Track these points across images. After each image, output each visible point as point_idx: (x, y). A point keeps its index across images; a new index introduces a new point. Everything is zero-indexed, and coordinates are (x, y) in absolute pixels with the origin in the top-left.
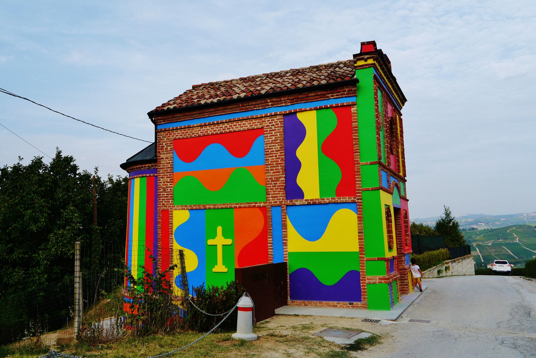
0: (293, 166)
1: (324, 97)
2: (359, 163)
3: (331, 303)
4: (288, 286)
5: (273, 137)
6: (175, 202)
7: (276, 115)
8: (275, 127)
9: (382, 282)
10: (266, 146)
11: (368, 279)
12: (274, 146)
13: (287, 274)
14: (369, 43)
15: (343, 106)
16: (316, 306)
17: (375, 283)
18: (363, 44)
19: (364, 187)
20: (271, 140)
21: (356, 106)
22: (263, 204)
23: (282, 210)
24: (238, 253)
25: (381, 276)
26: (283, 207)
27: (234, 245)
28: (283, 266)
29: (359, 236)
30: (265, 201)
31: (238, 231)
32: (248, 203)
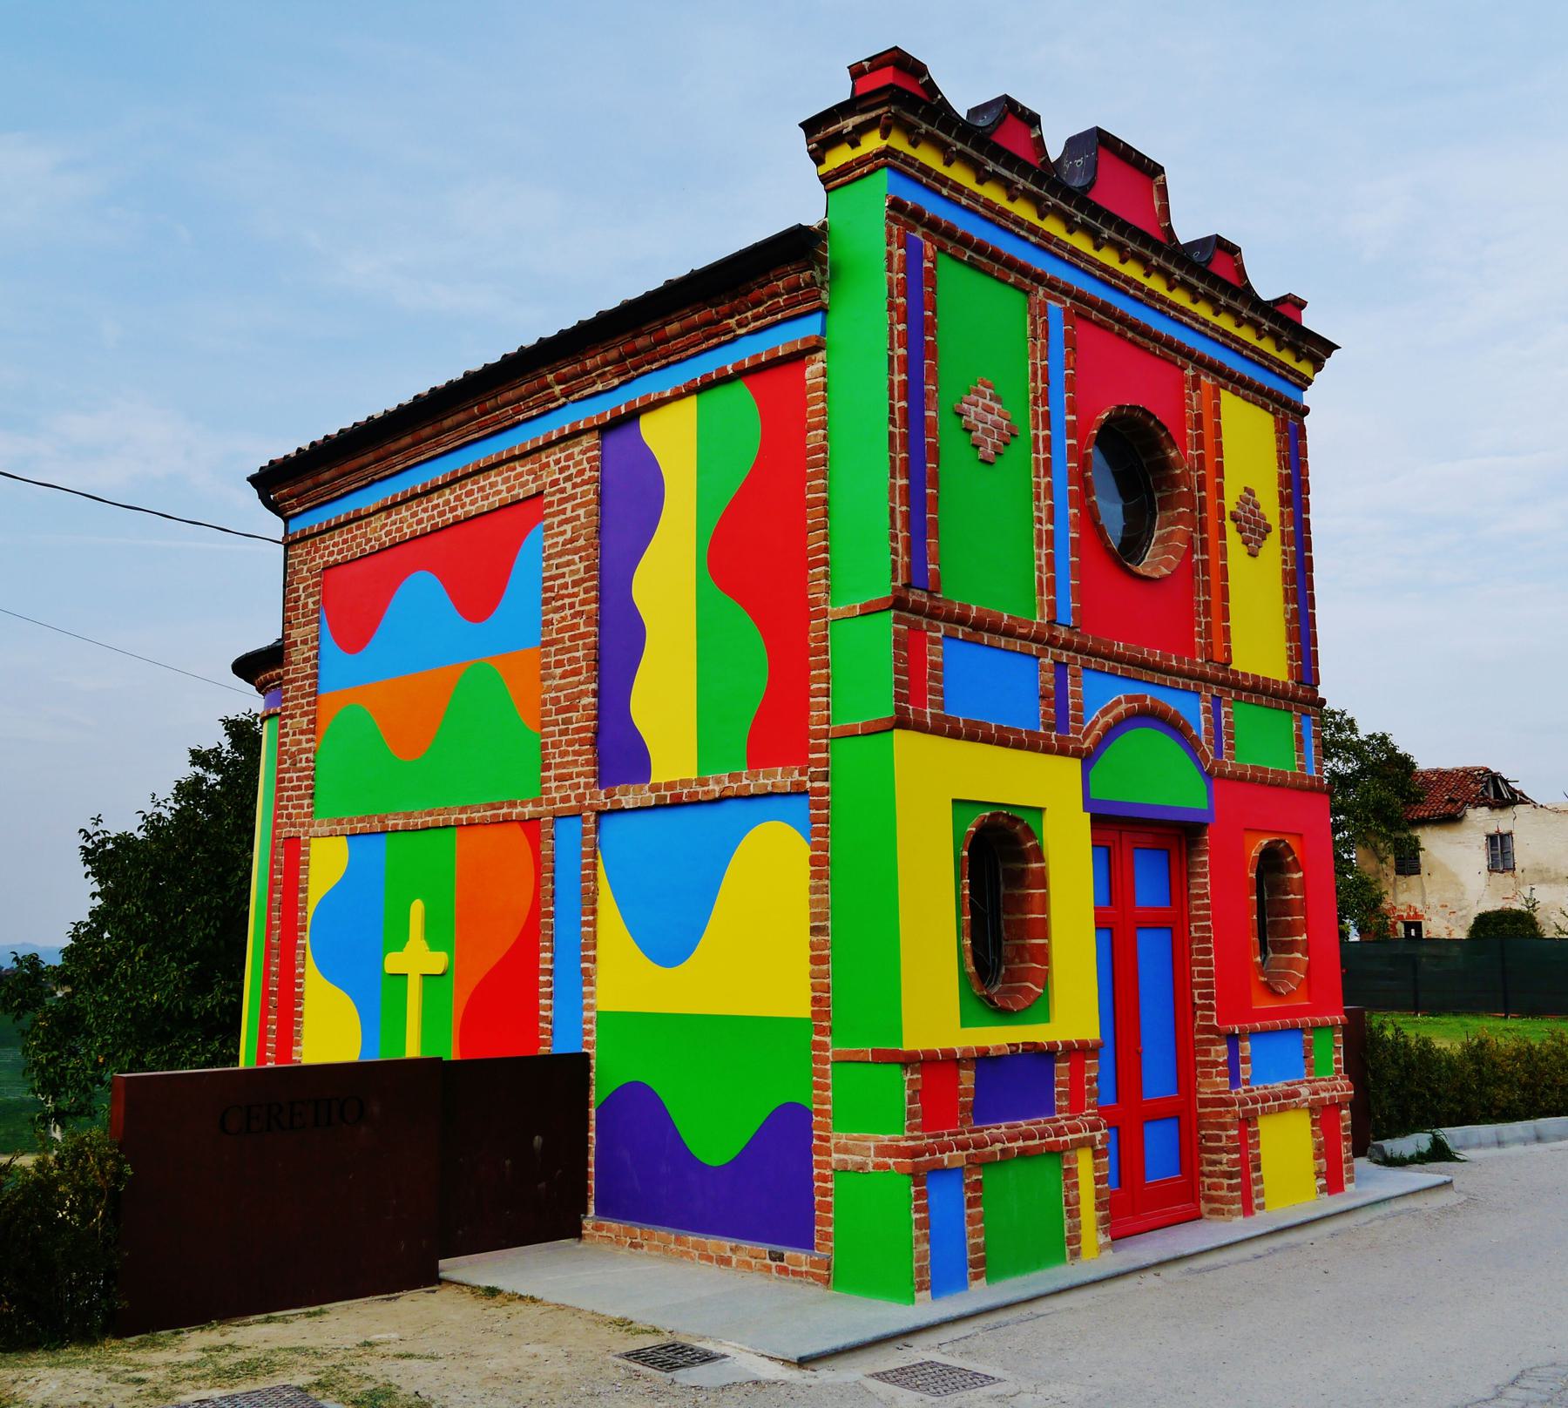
0: (618, 642)
1: (715, 335)
2: (824, 613)
3: (714, 1243)
4: (592, 1158)
5: (568, 527)
6: (319, 807)
7: (576, 434)
8: (575, 486)
9: (887, 1167)
10: (549, 568)
11: (838, 1150)
12: (568, 564)
13: (587, 1104)
14: (878, 61)
15: (776, 363)
16: (960, 899)
17: (861, 1167)
18: (857, 72)
20: (561, 539)
21: (820, 356)
22: (530, 808)
23: (585, 832)
24: (465, 998)
25: (885, 1139)
26: (586, 820)
27: (451, 976)
28: (578, 1064)
29: (813, 946)
30: (537, 795)
31: (463, 923)
32: (492, 806)
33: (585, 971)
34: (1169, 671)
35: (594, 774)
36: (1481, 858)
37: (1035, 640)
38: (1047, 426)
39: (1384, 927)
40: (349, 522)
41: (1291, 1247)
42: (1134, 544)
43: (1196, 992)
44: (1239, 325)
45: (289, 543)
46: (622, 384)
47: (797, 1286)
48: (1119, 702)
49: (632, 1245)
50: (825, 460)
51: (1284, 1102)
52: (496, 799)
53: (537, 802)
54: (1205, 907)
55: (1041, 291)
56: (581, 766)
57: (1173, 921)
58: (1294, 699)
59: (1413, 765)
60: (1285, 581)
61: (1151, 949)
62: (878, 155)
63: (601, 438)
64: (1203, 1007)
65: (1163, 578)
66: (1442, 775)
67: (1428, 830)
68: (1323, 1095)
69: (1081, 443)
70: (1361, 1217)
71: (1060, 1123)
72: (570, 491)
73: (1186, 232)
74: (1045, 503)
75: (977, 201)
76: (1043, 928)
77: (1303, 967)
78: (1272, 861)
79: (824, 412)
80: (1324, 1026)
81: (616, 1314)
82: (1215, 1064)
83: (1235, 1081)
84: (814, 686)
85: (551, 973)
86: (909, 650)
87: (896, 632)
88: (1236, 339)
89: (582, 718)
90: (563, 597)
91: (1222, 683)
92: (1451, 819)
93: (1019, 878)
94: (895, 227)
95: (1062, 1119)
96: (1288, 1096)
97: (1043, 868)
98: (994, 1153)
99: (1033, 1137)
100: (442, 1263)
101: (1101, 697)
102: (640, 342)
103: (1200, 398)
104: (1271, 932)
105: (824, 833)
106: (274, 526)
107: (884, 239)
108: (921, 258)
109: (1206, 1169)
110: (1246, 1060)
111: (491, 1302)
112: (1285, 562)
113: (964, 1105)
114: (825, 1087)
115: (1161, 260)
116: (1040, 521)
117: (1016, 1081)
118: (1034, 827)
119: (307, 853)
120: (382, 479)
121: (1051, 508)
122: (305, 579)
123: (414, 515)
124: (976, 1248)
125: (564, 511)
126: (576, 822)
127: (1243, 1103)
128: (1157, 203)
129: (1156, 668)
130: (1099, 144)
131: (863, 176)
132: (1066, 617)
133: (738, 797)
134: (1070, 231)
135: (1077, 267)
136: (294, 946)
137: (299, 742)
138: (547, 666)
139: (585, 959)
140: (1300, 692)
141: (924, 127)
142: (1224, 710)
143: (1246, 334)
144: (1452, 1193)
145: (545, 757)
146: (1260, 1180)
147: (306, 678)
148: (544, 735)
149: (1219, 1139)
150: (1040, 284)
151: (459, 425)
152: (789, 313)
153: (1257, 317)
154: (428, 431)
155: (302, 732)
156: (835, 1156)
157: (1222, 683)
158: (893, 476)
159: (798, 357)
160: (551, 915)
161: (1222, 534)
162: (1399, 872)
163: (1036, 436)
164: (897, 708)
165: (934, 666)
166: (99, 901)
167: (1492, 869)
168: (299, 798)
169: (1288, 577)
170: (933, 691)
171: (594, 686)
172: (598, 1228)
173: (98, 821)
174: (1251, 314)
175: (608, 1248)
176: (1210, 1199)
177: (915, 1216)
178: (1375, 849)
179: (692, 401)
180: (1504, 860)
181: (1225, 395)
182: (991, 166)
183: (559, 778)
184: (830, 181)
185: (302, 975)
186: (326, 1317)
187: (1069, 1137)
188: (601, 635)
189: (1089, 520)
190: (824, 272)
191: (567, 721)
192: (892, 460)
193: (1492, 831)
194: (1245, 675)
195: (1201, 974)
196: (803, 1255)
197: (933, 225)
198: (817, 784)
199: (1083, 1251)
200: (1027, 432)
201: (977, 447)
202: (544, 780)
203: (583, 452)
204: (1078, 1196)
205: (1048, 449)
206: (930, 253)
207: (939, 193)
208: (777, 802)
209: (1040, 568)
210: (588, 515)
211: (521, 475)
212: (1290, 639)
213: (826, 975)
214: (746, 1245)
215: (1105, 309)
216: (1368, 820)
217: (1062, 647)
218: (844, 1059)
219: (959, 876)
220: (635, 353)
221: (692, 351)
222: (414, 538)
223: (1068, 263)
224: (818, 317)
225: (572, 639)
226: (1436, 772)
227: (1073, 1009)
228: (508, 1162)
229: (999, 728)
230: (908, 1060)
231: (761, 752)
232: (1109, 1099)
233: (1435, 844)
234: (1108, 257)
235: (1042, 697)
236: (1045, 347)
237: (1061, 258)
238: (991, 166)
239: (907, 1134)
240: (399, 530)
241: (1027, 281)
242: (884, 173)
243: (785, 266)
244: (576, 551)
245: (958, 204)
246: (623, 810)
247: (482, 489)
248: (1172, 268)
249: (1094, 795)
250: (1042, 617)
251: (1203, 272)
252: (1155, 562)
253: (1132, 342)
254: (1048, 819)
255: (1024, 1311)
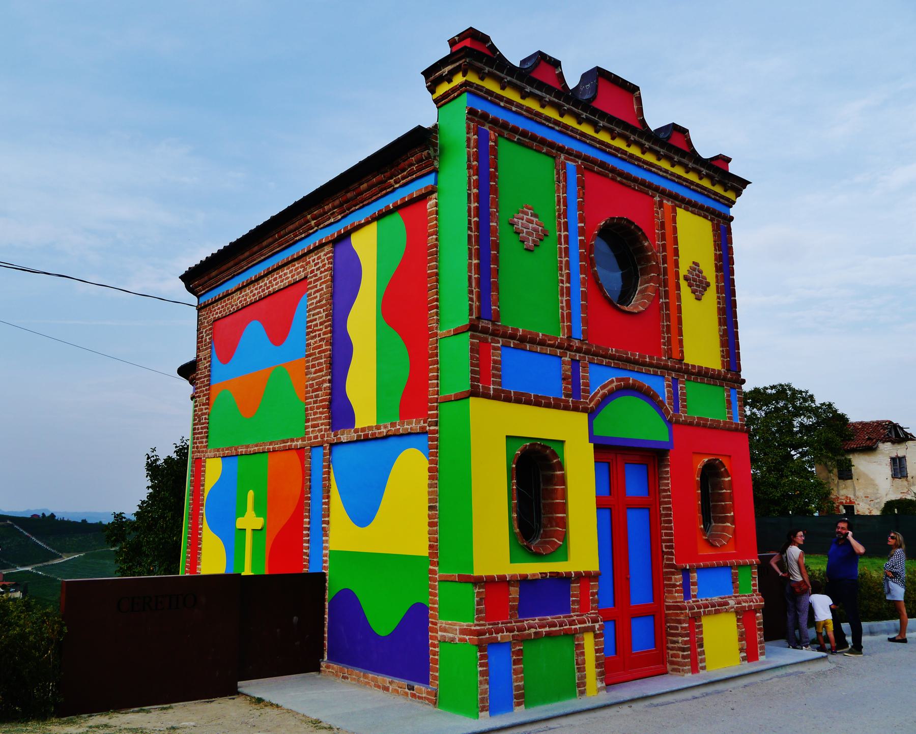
1: (385, 189)
2: (436, 335)
4: (326, 629)
5: (318, 294)
7: (321, 246)
8: (321, 273)
9: (465, 640)
13: (324, 600)
14: (463, 36)
16: (510, 491)
17: (452, 640)
18: (452, 43)
19: (444, 393)
20: (315, 301)
21: (434, 196)
23: (325, 455)
25: (464, 624)
26: (325, 448)
27: (265, 529)
28: (320, 579)
29: (430, 517)
31: (270, 505)
32: (284, 441)
33: (324, 529)
34: (644, 364)
35: (329, 424)
36: (887, 471)
37: (559, 347)
38: (566, 229)
39: (832, 508)
40: (224, 297)
41: (718, 692)
42: (626, 295)
43: (664, 545)
44: (687, 172)
45: (200, 309)
46: (343, 218)
47: (420, 705)
48: (612, 382)
49: (344, 677)
50: (437, 252)
51: (719, 609)
52: (285, 438)
53: (303, 439)
54: (669, 496)
55: (562, 157)
56: (322, 419)
57: (650, 505)
58: (725, 379)
59: (847, 420)
60: (719, 314)
61: (636, 521)
62: (462, 85)
63: (334, 247)
64: (668, 553)
65: (640, 313)
66: (864, 425)
67: (856, 455)
68: (744, 604)
69: (587, 239)
70: (765, 676)
71: (574, 618)
72: (319, 276)
73: (654, 123)
74: (565, 272)
75: (522, 109)
76: (564, 508)
77: (731, 531)
78: (711, 472)
79: (436, 226)
80: (745, 565)
81: (314, 717)
82: (674, 586)
83: (687, 596)
84: (431, 374)
85: (308, 529)
86: (479, 354)
87: (472, 344)
88: (686, 180)
89: (323, 395)
90: (315, 331)
91: (679, 370)
92: (869, 449)
93: (550, 480)
94: (472, 124)
95: (574, 616)
96: (720, 605)
97: (563, 474)
98: (530, 635)
99: (555, 626)
100: (240, 683)
101: (600, 379)
102: (349, 195)
103: (663, 212)
104: (710, 509)
105: (435, 454)
106: (194, 300)
107: (465, 130)
108: (488, 140)
109: (671, 645)
110: (694, 584)
111: (256, 707)
112: (719, 303)
113: (513, 607)
114: (435, 595)
115: (636, 138)
116: (562, 282)
117: (547, 594)
118: (557, 451)
119: (204, 466)
120: (238, 274)
121: (568, 275)
122: (206, 327)
123: (252, 292)
124: (518, 688)
125: (316, 286)
126: (320, 449)
127: (691, 608)
128: (635, 107)
129: (636, 362)
130: (598, 76)
131: (455, 98)
132: (578, 333)
133: (394, 435)
134: (580, 123)
135: (585, 143)
136: (198, 514)
137: (202, 410)
138: (308, 368)
139: (324, 522)
140: (730, 373)
141: (487, 69)
142: (680, 386)
143: (692, 177)
144: (827, 663)
145: (307, 415)
146: (703, 653)
147: (205, 377)
148: (307, 404)
149: (677, 628)
150: (544, 145)
151: (270, 244)
152: (419, 174)
153: (698, 167)
154: (256, 248)
155: (204, 405)
156: (440, 633)
157: (679, 370)
158: (470, 258)
159: (423, 197)
160: (309, 498)
161: (678, 287)
162: (840, 478)
163: (560, 235)
164: (472, 386)
165: (495, 362)
166: (151, 490)
167: (894, 476)
168: (202, 438)
169: (721, 311)
170: (494, 376)
171: (329, 377)
172: (328, 667)
173: (154, 450)
174: (695, 166)
175: (332, 678)
176: (672, 663)
177: (479, 669)
178: (826, 464)
179: (374, 226)
180: (901, 471)
181: (680, 211)
182: (528, 89)
183: (314, 426)
184: (440, 102)
185: (201, 529)
186: (170, 711)
187: (578, 626)
188: (333, 350)
189: (594, 281)
190: (435, 151)
191: (317, 396)
192: (470, 250)
193: (894, 455)
194: (693, 366)
195: (666, 534)
196: (423, 688)
197: (495, 122)
198: (432, 428)
199: (587, 691)
200: (554, 233)
201: (523, 242)
202: (307, 427)
203: (325, 255)
204: (584, 660)
205: (567, 242)
206: (493, 137)
207: (499, 105)
208: (413, 438)
209: (562, 308)
210: (327, 287)
211: (297, 268)
212: (722, 345)
213: (436, 532)
214: (396, 680)
215: (602, 165)
216: (821, 450)
217: (575, 351)
218: (445, 580)
219: (510, 478)
220: (346, 201)
221: (375, 198)
222: (252, 304)
223: (580, 140)
224: (433, 176)
225: (319, 353)
226: (861, 423)
227: (583, 551)
228: (278, 630)
229: (536, 396)
230: (477, 581)
231: (406, 412)
232: (608, 603)
233: (861, 463)
234: (604, 137)
235: (564, 379)
236: (565, 187)
237: (575, 138)
238: (528, 89)
239: (476, 622)
240: (245, 300)
241: (554, 151)
242: (465, 95)
243: (417, 146)
244: (321, 307)
245: (511, 110)
246: (342, 443)
247: (280, 277)
248: (643, 141)
249: (597, 432)
250: (564, 335)
251: (664, 144)
252: (637, 304)
253: (621, 183)
254: (567, 448)
255: (542, 726)
